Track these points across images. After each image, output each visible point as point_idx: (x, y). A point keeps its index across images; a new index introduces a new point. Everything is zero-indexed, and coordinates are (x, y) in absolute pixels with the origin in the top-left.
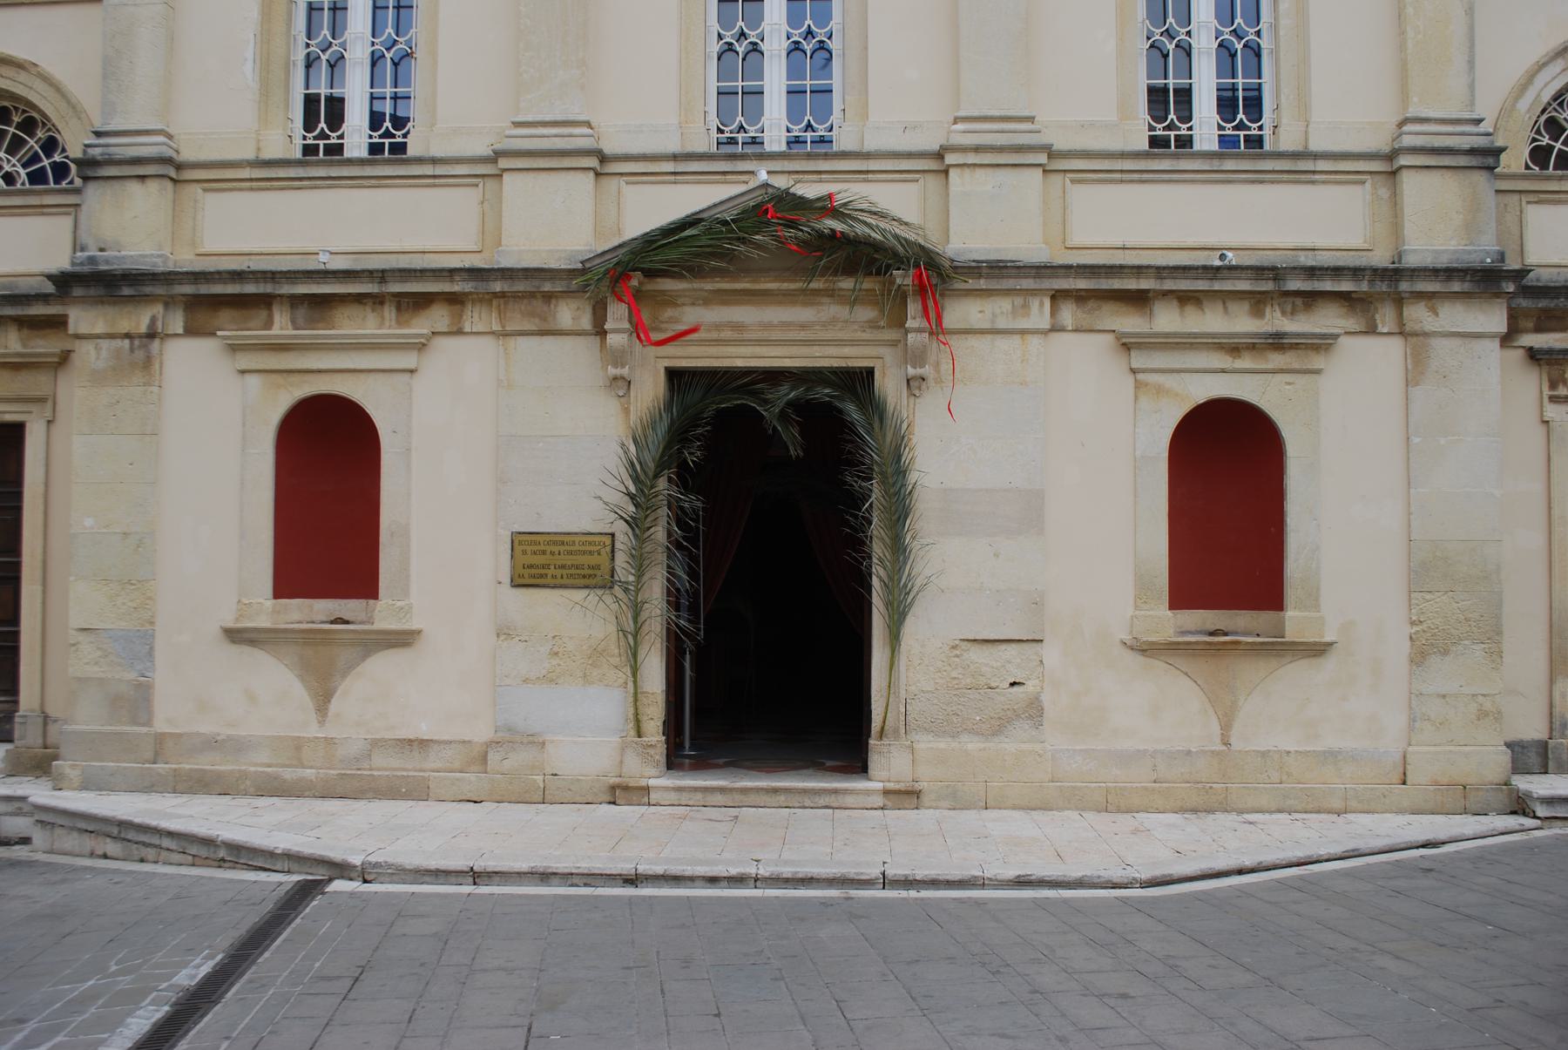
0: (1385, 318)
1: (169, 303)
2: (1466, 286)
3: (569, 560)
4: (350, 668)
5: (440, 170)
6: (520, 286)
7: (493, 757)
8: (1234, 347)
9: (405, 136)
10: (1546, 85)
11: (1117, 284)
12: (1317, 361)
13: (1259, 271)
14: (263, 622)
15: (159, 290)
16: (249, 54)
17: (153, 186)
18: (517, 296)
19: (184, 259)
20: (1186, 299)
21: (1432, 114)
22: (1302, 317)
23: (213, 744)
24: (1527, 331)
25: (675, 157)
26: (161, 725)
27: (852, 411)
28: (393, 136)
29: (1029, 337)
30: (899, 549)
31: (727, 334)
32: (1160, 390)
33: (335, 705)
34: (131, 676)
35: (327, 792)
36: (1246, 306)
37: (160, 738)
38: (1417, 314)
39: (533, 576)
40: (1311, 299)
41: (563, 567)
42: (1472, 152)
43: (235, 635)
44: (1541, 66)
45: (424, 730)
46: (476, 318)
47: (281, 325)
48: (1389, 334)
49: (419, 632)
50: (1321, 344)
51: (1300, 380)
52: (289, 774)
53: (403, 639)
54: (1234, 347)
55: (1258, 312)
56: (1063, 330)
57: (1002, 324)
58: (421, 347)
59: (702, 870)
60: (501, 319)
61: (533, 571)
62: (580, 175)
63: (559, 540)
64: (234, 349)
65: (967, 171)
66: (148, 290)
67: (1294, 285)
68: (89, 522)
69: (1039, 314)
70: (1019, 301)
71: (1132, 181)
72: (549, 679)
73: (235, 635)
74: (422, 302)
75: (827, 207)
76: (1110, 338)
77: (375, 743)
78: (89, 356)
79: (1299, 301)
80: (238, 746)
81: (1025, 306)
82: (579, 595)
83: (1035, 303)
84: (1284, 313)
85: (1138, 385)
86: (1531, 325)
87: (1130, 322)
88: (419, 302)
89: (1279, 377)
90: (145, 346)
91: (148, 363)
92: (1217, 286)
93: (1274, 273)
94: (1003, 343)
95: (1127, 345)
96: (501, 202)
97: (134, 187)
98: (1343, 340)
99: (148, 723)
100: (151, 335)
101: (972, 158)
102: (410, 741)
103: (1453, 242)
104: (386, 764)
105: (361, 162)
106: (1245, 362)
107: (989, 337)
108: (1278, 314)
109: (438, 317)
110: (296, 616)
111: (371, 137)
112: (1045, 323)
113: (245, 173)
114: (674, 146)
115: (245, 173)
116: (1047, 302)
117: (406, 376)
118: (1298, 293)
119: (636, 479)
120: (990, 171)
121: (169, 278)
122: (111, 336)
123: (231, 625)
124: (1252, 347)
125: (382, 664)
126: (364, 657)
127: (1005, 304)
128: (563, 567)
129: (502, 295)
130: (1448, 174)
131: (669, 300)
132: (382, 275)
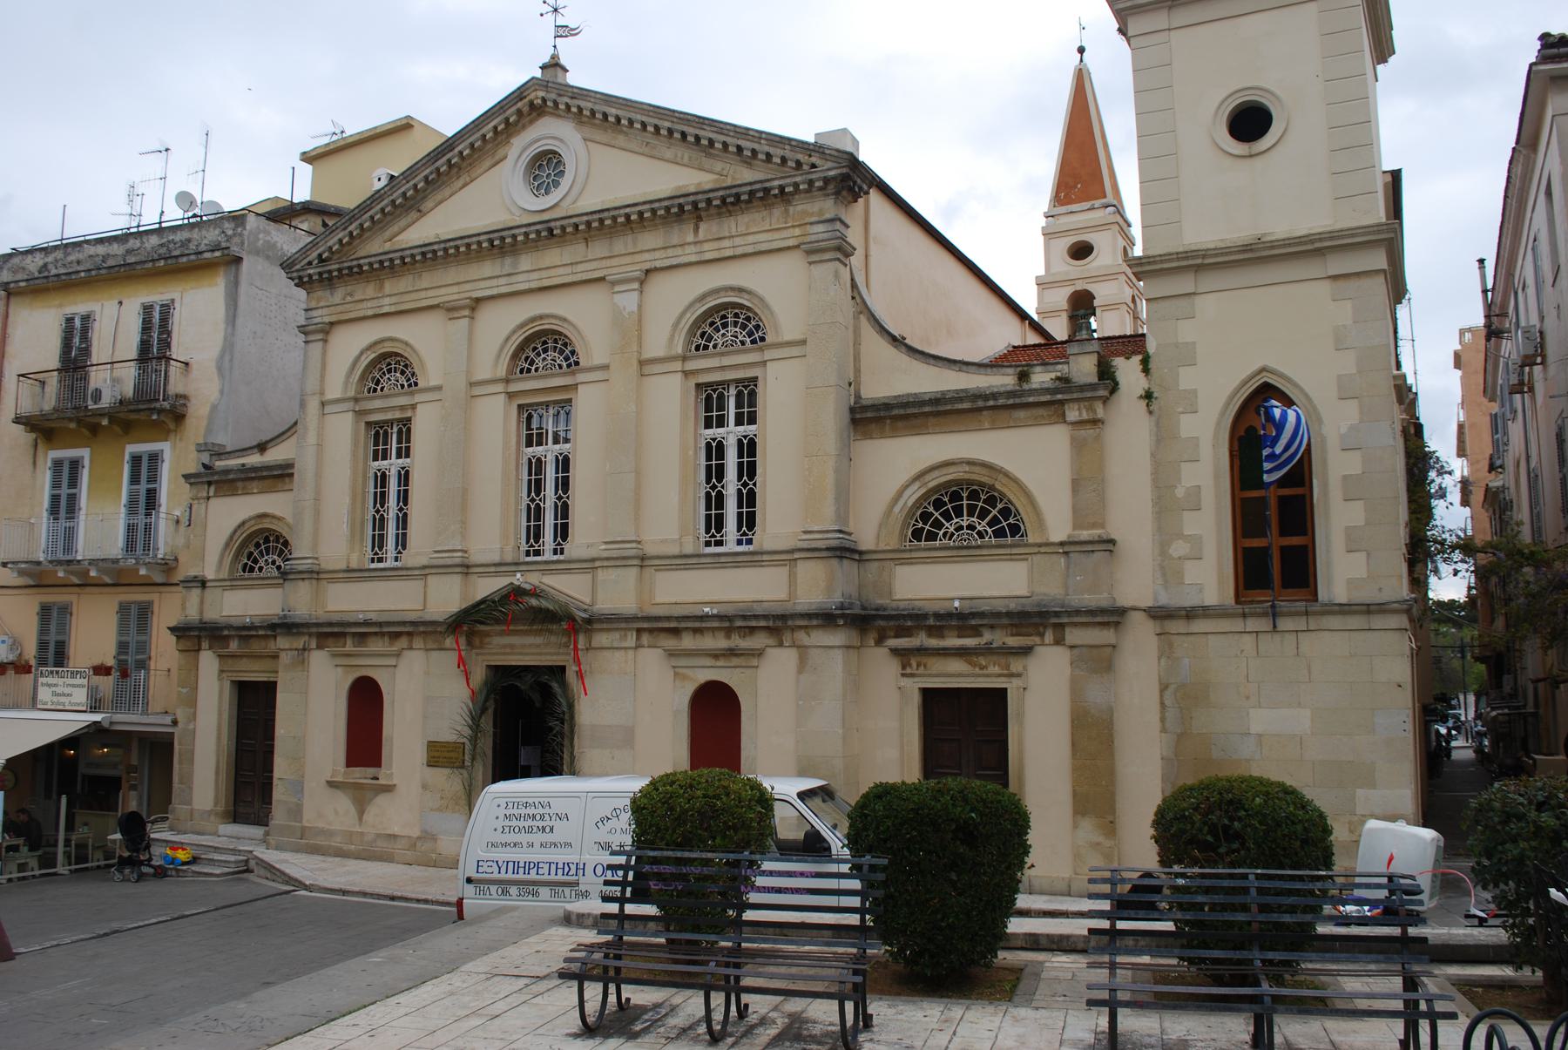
1: (310, 635)
2: (820, 622)
4: (371, 800)
5: (409, 573)
6: (430, 629)
7: (419, 844)
8: (716, 655)
12: (754, 662)
14: (340, 779)
15: (305, 630)
16: (345, 520)
17: (307, 582)
18: (431, 633)
19: (320, 615)
20: (696, 631)
21: (816, 528)
22: (748, 639)
23: (322, 832)
24: (890, 637)
25: (495, 565)
26: (306, 824)
27: (555, 685)
31: (508, 650)
33: (365, 817)
34: (296, 800)
35: (358, 856)
37: (304, 829)
38: (802, 637)
40: (752, 630)
42: (828, 549)
43: (331, 784)
44: (906, 487)
45: (396, 830)
46: (418, 642)
47: (349, 647)
49: (395, 785)
50: (759, 653)
51: (748, 672)
52: (345, 847)
53: (389, 789)
54: (716, 655)
55: (728, 637)
56: (643, 647)
58: (398, 655)
59: (413, 896)
60: (425, 643)
62: (455, 576)
64: (334, 655)
66: (301, 630)
67: (739, 623)
68: (282, 731)
70: (623, 633)
72: (440, 810)
73: (331, 784)
74: (396, 635)
75: (535, 593)
77: (378, 835)
78: (285, 658)
79: (747, 630)
80: (330, 834)
81: (626, 635)
82: (447, 771)
83: (629, 634)
85: (676, 674)
86: (892, 634)
87: (670, 643)
88: (395, 636)
90: (302, 654)
91: (303, 662)
94: (617, 654)
95: (672, 654)
97: (301, 583)
98: (768, 650)
99: (301, 822)
100: (304, 649)
101: (606, 564)
102: (390, 835)
104: (382, 845)
106: (721, 663)
109: (403, 642)
110: (358, 775)
112: (633, 644)
113: (341, 575)
114: (497, 559)
115: (341, 575)
116: (635, 634)
117: (392, 669)
119: (473, 719)
120: (614, 569)
121: (307, 625)
122: (291, 650)
123: (329, 779)
124: (723, 655)
125: (382, 800)
126: (376, 796)
127: (617, 635)
129: (423, 632)
130: (819, 561)
131: (487, 634)
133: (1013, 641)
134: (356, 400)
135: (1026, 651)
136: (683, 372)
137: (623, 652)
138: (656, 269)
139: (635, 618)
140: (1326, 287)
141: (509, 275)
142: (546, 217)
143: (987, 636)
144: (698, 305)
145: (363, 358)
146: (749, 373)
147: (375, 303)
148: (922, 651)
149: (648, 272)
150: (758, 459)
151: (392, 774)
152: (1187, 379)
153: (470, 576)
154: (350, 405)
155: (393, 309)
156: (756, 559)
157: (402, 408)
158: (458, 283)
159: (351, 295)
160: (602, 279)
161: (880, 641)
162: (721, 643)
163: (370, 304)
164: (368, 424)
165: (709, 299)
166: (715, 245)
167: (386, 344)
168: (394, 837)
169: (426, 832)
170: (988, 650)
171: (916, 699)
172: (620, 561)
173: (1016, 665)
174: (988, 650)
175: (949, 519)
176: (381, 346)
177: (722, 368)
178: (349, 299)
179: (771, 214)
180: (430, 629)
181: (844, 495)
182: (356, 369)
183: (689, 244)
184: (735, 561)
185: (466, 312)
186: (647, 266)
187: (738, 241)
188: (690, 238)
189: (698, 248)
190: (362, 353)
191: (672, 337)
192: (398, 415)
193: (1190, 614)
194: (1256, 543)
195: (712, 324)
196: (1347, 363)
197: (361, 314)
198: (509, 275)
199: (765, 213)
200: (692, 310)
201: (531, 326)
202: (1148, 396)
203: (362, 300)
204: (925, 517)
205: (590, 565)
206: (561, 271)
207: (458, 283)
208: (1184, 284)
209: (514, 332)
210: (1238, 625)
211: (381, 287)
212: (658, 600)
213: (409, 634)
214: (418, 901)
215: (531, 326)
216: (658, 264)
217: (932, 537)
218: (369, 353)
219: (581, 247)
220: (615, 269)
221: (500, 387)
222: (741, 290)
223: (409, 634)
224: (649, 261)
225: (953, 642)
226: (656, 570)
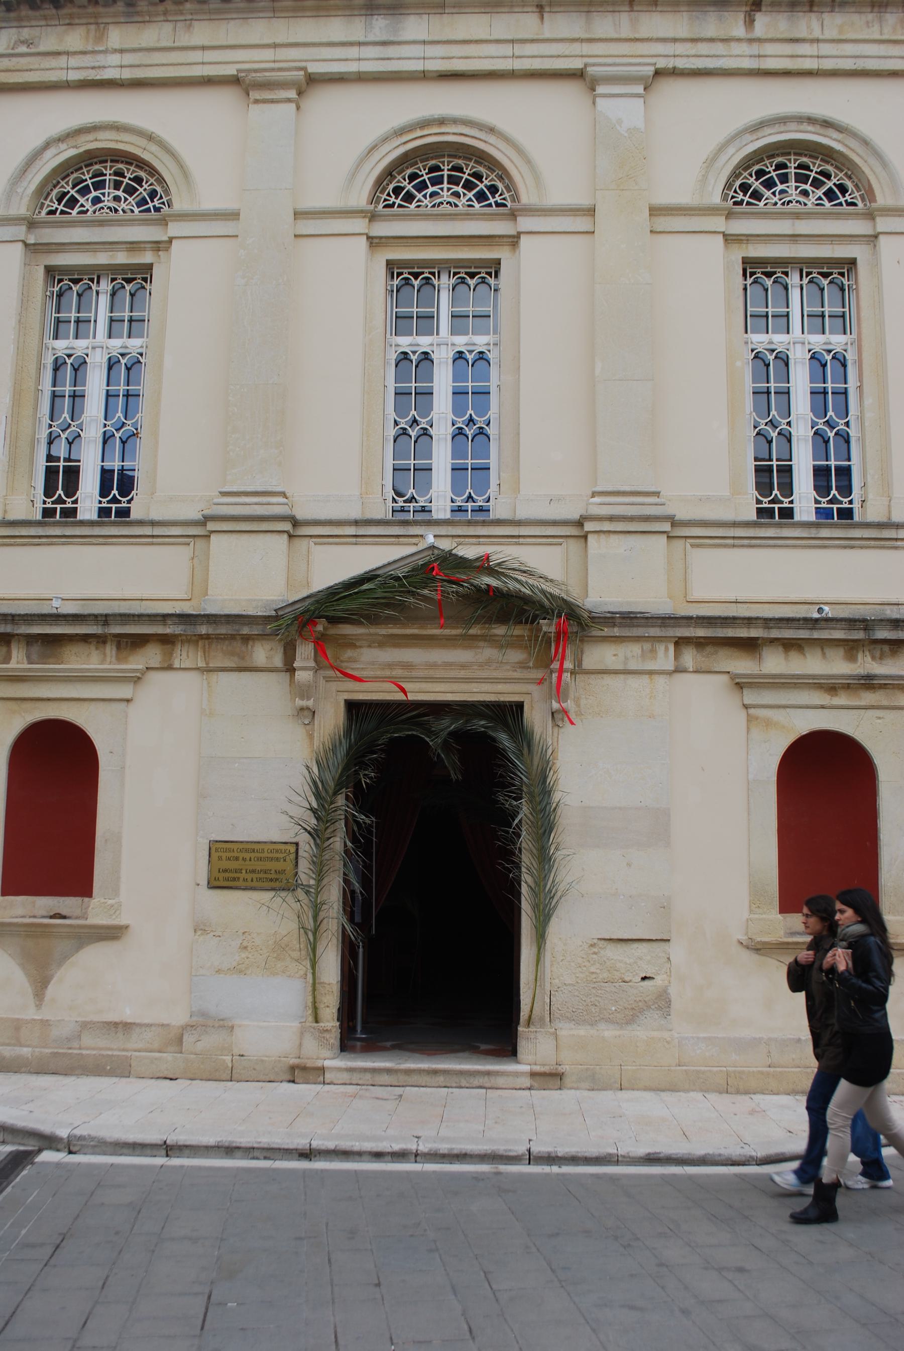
3: (259, 866)
4: (65, 958)
5: (158, 531)
6: (223, 630)
7: (188, 1039)
8: (832, 686)
9: (129, 502)
11: (730, 633)
13: (851, 623)
18: (219, 638)
20: (789, 645)
25: (356, 523)
27: (504, 739)
29: (656, 677)
30: (544, 858)
32: (768, 724)
35: (41, 1068)
36: (841, 652)
39: (227, 879)
41: (253, 871)
45: (127, 1014)
46: (184, 656)
49: (127, 927)
54: (832, 686)
55: (851, 657)
56: (685, 671)
57: (633, 666)
58: (136, 679)
61: (227, 875)
62: (275, 537)
63: (251, 848)
65: (603, 536)
69: (665, 657)
70: (647, 646)
71: (787, 546)
72: (239, 970)
74: (138, 642)
75: (484, 565)
76: (724, 678)
79: (886, 648)
81: (653, 651)
83: (661, 648)
84: (873, 658)
85: (750, 719)
87: (742, 665)
89: (870, 713)
93: (865, 624)
94: (634, 682)
95: (740, 684)
101: (607, 526)
102: (116, 1024)
105: (91, 523)
106: (841, 699)
107: (622, 676)
108: (869, 659)
109: (152, 655)
110: (20, 912)
111: (819, 503)
112: (670, 665)
116: (671, 648)
117: (124, 704)
119: (318, 795)
120: (622, 537)
124: (848, 687)
127: (635, 649)
128: (253, 871)
129: (207, 637)
132: (105, 619)
134: (32, 225)
136: (725, 235)
137: (645, 679)
138: (675, 73)
139: (666, 621)
141: (384, 43)
144: (748, 137)
145: (49, 153)
147: (88, 61)
149: (658, 73)
151: (120, 904)
153: (297, 541)
154: (20, 231)
155: (127, 74)
157: (133, 246)
158: (275, 46)
159: (28, 43)
160: (578, 75)
163: (74, 61)
164: (51, 272)
165: (768, 131)
166: (788, 49)
167: (102, 135)
168: (126, 1027)
169: (204, 1014)
176: (91, 137)
177: (794, 238)
178: (23, 49)
179: (881, 21)
180: (223, 630)
182: (29, 175)
183: (739, 40)
185: (292, 94)
186: (662, 63)
187: (826, 49)
188: (739, 30)
189: (755, 49)
190: (47, 145)
191: (704, 179)
192: (121, 258)
195: (760, 174)
197: (53, 76)
198: (384, 43)
199: (870, 17)
200: (737, 143)
201: (419, 133)
203: (58, 54)
206: (491, 49)
207: (275, 46)
209: (385, 139)
211: (101, 37)
212: (697, 595)
213: (166, 640)
214: (378, 1156)
215: (419, 133)
216: (681, 64)
218: (63, 146)
221: (360, 225)
223: (166, 640)
226: (692, 546)
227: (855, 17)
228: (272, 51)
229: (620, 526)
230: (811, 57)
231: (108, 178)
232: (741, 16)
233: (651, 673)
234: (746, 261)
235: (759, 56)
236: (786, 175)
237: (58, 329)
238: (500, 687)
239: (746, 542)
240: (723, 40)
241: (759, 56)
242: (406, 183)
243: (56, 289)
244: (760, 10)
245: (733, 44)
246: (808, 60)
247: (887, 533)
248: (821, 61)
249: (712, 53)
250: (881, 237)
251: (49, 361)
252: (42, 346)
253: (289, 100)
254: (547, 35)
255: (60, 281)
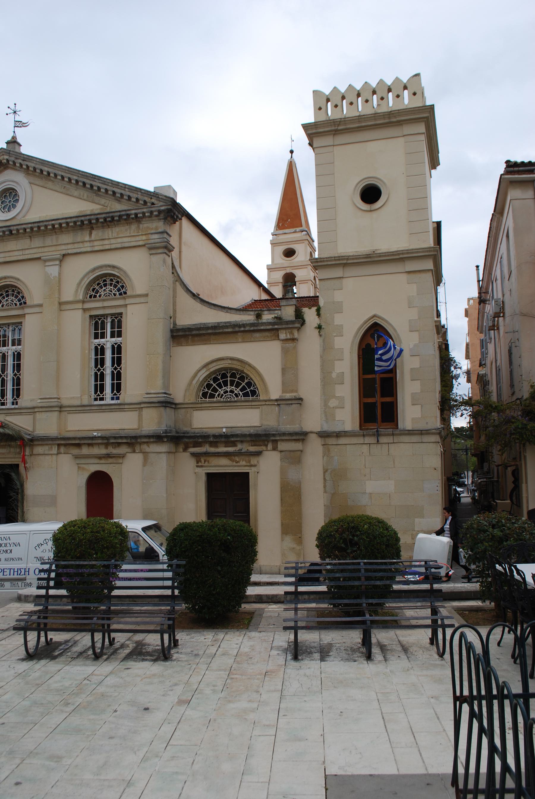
0: (137, 448)
2: (154, 440)
8: (100, 457)
9: (120, 395)
10: (201, 376)
11: (74, 442)
12: (120, 461)
20: (89, 445)
21: (152, 392)
27: (13, 474)
28: (117, 395)
29: (53, 456)
32: (84, 469)
36: (104, 446)
38: (145, 447)
40: (119, 444)
44: (199, 371)
48: (139, 452)
50: (123, 456)
51: (117, 465)
54: (100, 457)
55: (106, 448)
56: (61, 453)
57: (46, 453)
65: (40, 413)
67: (112, 441)
70: (50, 446)
71: (94, 412)
76: (70, 455)
79: (116, 444)
81: (52, 448)
83: (53, 447)
84: (113, 448)
85: (79, 468)
86: (192, 445)
87: (76, 451)
89: (112, 465)
92: (94, 442)
96: (283, 382)
98: (128, 454)
101: (41, 410)
103: (155, 427)
106: (103, 461)
107: (44, 456)
108: (111, 448)
116: (56, 447)
118: (113, 443)
120: (45, 412)
124: (104, 457)
127: (47, 448)
133: (252, 449)
135: (258, 454)
137: (50, 456)
138: (69, 254)
139: (56, 439)
140: (404, 277)
142: (8, 224)
143: (239, 446)
144: (91, 274)
146: (118, 311)
148: (207, 454)
150: (123, 355)
152: (338, 319)
156: (121, 407)
161: (185, 450)
162: (103, 451)
170: (239, 453)
171: (204, 478)
172: (48, 409)
173: (254, 461)
174: (239, 453)
175: (221, 387)
177: (104, 307)
181: (167, 375)
183: (86, 241)
184: (110, 408)
185: (58, 262)
186: (64, 252)
187: (113, 241)
188: (87, 238)
189: (91, 244)
191: (77, 291)
193: (338, 435)
194: (370, 400)
196: (413, 314)
199: (127, 227)
200: (87, 277)
202: (319, 327)
204: (209, 386)
205: (32, 410)
206: (16, 253)
208: (338, 272)
210: (361, 440)
217: (212, 396)
219: (28, 241)
220: (47, 253)
222: (114, 267)
224: (64, 249)
225: (222, 449)
226: (68, 413)
227: (123, 228)
228: (72, 245)
229: (44, 409)
230: (108, 244)
231: (108, 282)
232: (88, 232)
233: (51, 454)
234: (91, 316)
235: (93, 246)
236: (117, 286)
237: (96, 337)
238: (13, 460)
239: (82, 411)
240: (82, 242)
241: (93, 246)
242: (120, 284)
243: (94, 322)
244: (94, 230)
245: (85, 243)
246: (107, 246)
247: (122, 407)
248: (111, 245)
249: (79, 247)
250: (128, 306)
251: (93, 347)
252: (90, 343)
253: (57, 265)
254: (33, 247)
255: (95, 319)
